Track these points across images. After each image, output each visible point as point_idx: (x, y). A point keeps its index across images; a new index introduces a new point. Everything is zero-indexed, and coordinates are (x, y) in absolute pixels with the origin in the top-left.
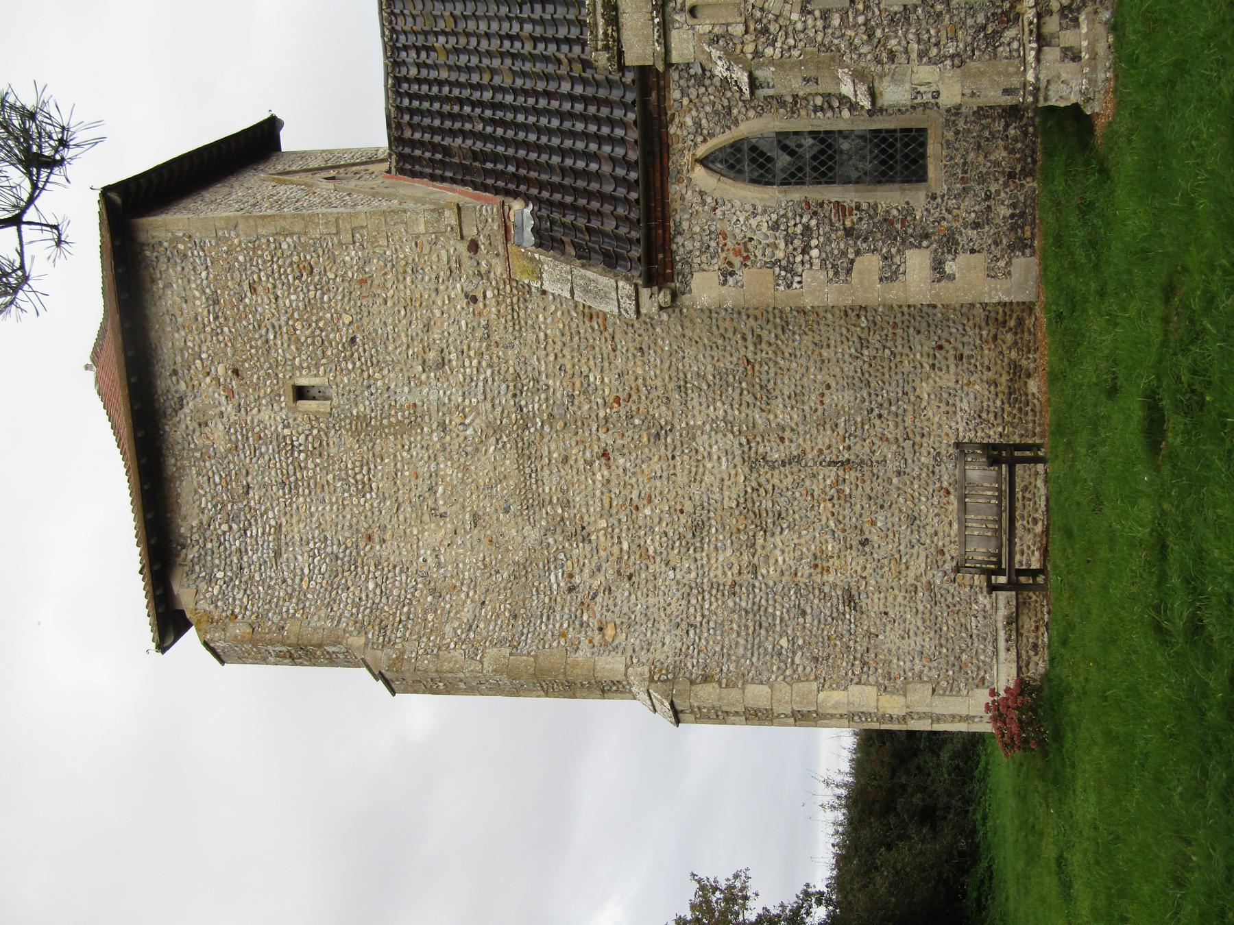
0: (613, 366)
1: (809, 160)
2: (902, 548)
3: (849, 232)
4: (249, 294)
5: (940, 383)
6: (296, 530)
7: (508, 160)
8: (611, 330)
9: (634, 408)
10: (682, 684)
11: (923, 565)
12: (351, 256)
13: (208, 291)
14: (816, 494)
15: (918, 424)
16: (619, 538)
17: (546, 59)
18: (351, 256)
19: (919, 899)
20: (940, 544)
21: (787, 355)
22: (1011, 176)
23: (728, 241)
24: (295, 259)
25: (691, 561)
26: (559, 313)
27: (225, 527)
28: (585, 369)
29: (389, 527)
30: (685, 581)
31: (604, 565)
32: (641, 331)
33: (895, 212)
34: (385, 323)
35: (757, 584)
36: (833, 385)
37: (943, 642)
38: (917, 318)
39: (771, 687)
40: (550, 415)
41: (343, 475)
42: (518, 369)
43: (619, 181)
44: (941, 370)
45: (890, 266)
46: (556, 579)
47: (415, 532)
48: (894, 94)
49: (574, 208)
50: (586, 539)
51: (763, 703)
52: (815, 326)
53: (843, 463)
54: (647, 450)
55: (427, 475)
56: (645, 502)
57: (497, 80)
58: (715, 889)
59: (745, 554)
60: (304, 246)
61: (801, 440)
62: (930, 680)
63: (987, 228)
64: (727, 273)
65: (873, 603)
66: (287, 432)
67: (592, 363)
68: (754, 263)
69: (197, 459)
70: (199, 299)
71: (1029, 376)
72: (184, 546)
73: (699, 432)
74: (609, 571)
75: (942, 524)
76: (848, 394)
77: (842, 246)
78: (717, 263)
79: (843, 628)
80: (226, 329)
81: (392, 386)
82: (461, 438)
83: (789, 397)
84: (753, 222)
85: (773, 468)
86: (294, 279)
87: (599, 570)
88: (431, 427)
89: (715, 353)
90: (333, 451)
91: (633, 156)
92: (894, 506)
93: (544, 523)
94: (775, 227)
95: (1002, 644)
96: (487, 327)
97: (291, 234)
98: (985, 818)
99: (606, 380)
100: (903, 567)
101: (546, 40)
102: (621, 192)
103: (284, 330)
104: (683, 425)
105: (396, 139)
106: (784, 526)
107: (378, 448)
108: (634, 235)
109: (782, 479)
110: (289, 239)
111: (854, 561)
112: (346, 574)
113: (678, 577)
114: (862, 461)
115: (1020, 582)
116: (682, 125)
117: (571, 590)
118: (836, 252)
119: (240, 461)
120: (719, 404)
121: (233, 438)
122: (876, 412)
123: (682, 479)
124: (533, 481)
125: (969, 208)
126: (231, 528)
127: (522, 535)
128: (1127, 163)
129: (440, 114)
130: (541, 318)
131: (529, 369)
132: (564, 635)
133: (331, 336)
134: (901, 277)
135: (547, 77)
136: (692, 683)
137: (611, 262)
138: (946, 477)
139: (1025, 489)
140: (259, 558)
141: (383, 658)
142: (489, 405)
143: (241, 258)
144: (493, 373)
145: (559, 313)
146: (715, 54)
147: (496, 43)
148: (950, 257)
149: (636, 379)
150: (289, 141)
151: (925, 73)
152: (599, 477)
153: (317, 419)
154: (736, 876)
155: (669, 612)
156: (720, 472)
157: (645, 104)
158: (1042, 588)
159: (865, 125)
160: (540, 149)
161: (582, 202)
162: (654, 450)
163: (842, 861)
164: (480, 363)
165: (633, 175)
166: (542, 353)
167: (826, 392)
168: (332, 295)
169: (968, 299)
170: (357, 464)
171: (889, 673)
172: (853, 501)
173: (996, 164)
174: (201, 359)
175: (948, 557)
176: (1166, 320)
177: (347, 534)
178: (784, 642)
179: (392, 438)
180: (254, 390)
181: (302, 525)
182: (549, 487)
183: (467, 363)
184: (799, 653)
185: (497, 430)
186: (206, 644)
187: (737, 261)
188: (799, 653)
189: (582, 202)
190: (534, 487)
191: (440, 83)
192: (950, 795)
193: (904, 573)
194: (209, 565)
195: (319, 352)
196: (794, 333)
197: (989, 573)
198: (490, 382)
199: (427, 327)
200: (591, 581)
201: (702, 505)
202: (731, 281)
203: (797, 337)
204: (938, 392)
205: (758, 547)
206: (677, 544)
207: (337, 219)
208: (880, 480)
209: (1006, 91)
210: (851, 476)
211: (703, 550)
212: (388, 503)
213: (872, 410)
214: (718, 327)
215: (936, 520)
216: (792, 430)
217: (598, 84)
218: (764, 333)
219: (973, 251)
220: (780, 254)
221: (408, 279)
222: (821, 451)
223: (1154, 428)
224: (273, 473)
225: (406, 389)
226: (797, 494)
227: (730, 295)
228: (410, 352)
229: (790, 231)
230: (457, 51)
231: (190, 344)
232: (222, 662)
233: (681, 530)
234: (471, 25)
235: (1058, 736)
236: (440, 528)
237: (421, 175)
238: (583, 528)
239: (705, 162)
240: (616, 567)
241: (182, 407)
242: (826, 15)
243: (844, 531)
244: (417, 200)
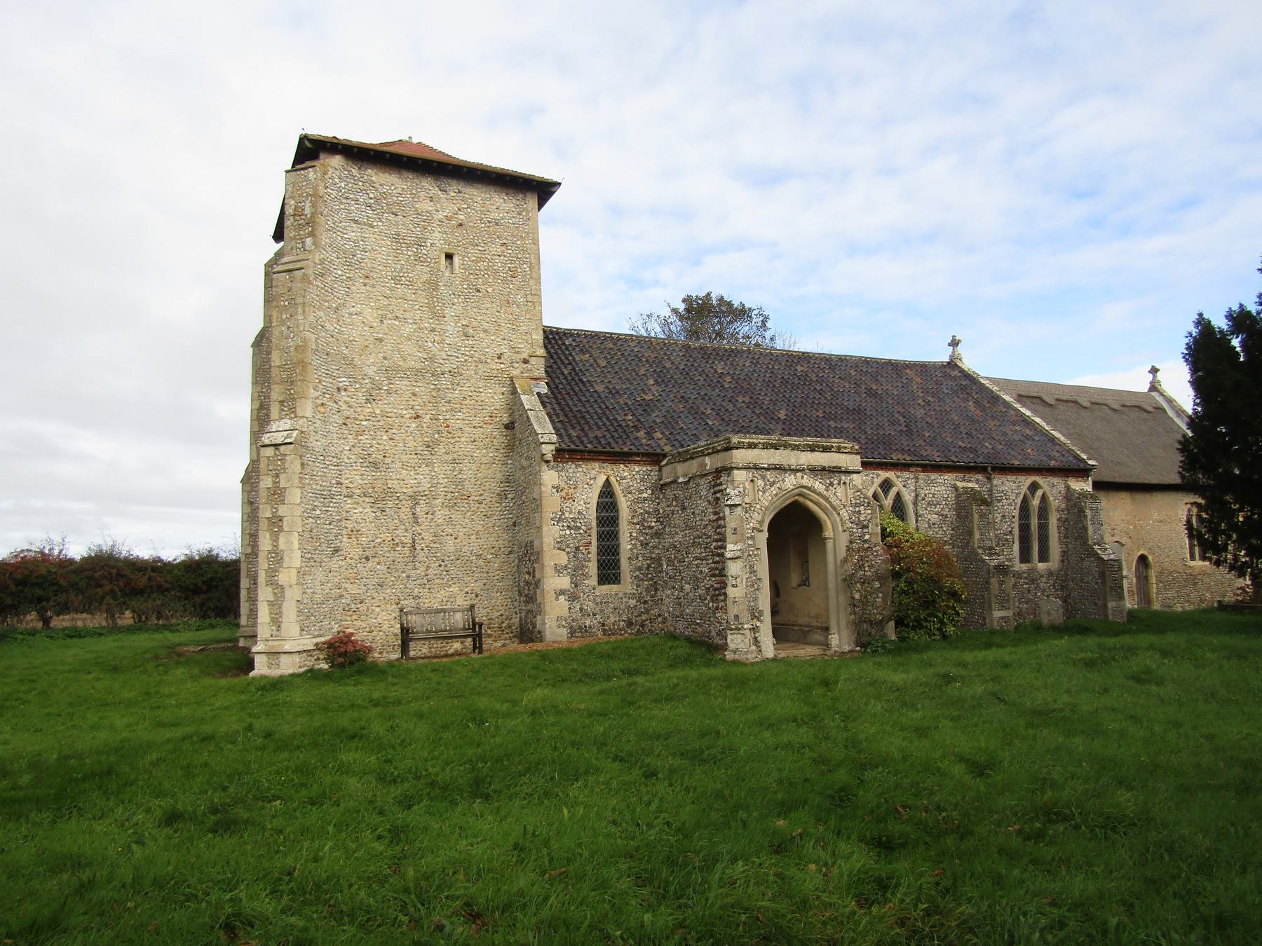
3: (577, 548)
50: (368, 401)
64: (558, 489)
65: (335, 564)
76: (452, 549)
78: (563, 485)
94: (580, 513)
109: (405, 513)
111: (356, 553)
123: (404, 458)
125: (589, 606)
127: (370, 365)
178: (318, 512)
187: (563, 494)
199: (485, 331)
210: (407, 551)
227: (547, 489)
239: (608, 482)
242: (752, 538)
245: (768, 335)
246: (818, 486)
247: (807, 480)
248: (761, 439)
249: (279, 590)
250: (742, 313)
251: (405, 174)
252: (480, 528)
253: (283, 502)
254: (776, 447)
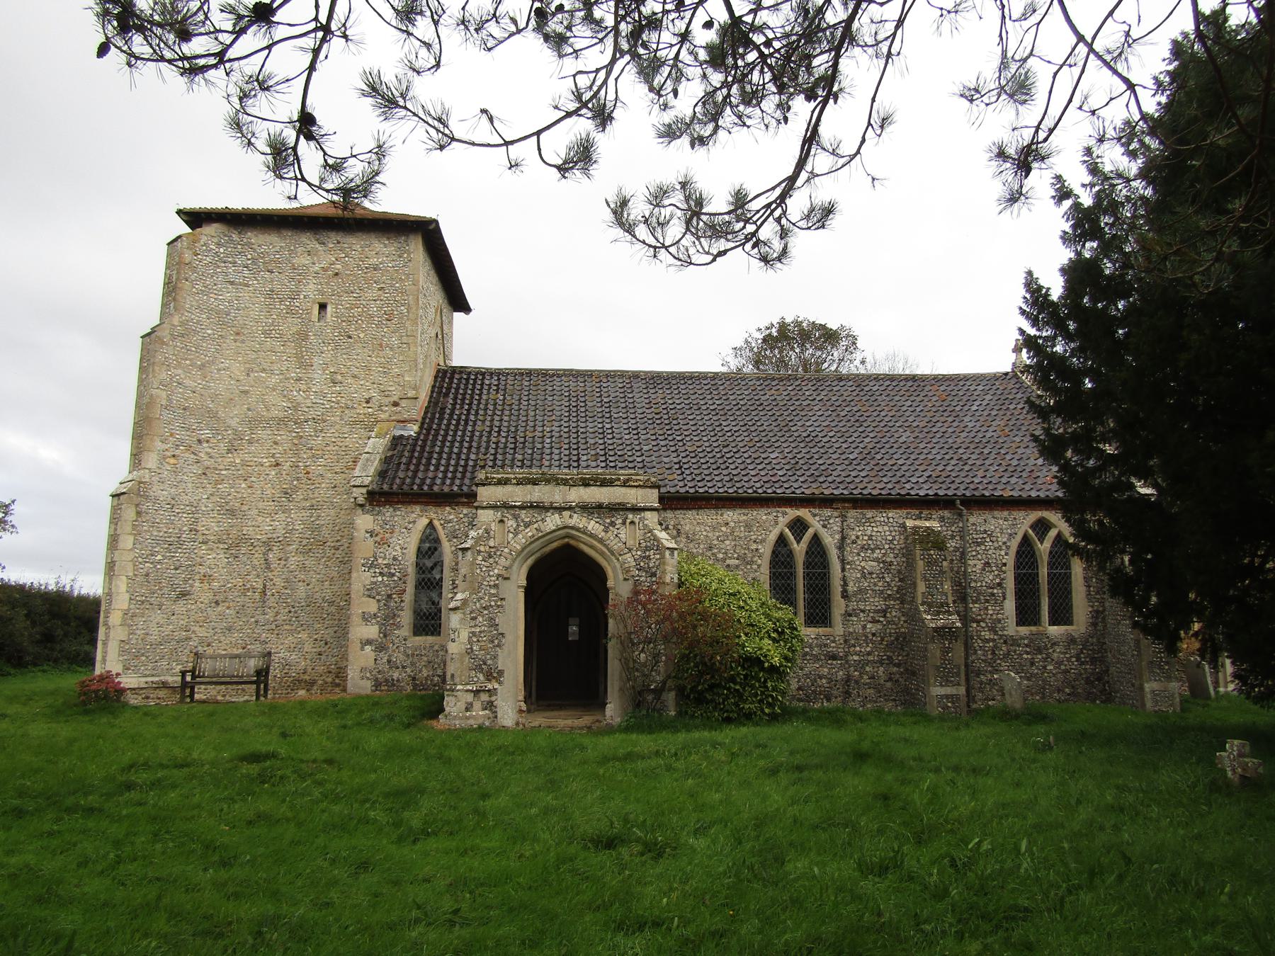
1: (429, 576)
3: (389, 596)
7: (439, 425)
10: (136, 500)
12: (395, 341)
17: (487, 448)
18: (395, 341)
19: (25, 633)
22: (414, 679)
38: (342, 632)
43: (423, 480)
46: (206, 433)
48: (454, 620)
49: (411, 457)
50: (229, 451)
51: (121, 545)
57: (479, 423)
58: (6, 514)
62: (130, 639)
65: (180, 607)
75: (226, 644)
78: (377, 529)
79: (166, 590)
84: (398, 548)
90: (290, 320)
91: (436, 488)
94: (395, 559)
95: (150, 679)
98: (44, 671)
101: (496, 449)
102: (418, 481)
105: (454, 370)
108: (395, 487)
109: (257, 559)
111: (207, 597)
115: (186, 688)
116: (450, 513)
117: (199, 441)
123: (261, 505)
125: (398, 657)
127: (234, 418)
128: (407, 738)
129: (465, 393)
132: (172, 435)
135: (478, 448)
136: (137, 505)
137: (382, 474)
139: (243, 690)
141: (165, 333)
146: (480, 531)
147: (497, 424)
150: (458, 316)
151: (464, 635)
154: (13, 526)
156: (262, 525)
157: (461, 495)
158: (182, 701)
159: (443, 603)
160: (443, 442)
161: (414, 461)
163: (21, 588)
165: (426, 488)
169: (350, 658)
173: (420, 671)
176: (314, 761)
178: (159, 557)
182: (262, 434)
185: (295, 409)
186: (179, 237)
187: (378, 539)
189: (414, 461)
191: (480, 395)
192: (61, 651)
197: (193, 671)
199: (354, 377)
204: (302, 643)
209: (453, 676)
217: (473, 473)
220: (380, 561)
223: (255, 758)
227: (360, 534)
230: (495, 405)
232: (169, 244)
234: (507, 413)
235: (86, 712)
237: (435, 381)
239: (431, 524)
242: (496, 586)
244: (422, 377)
245: (858, 356)
246: (593, 526)
247: (577, 520)
248: (520, 472)
250: (830, 337)
251: (285, 233)
252: (335, 574)
254: (534, 482)
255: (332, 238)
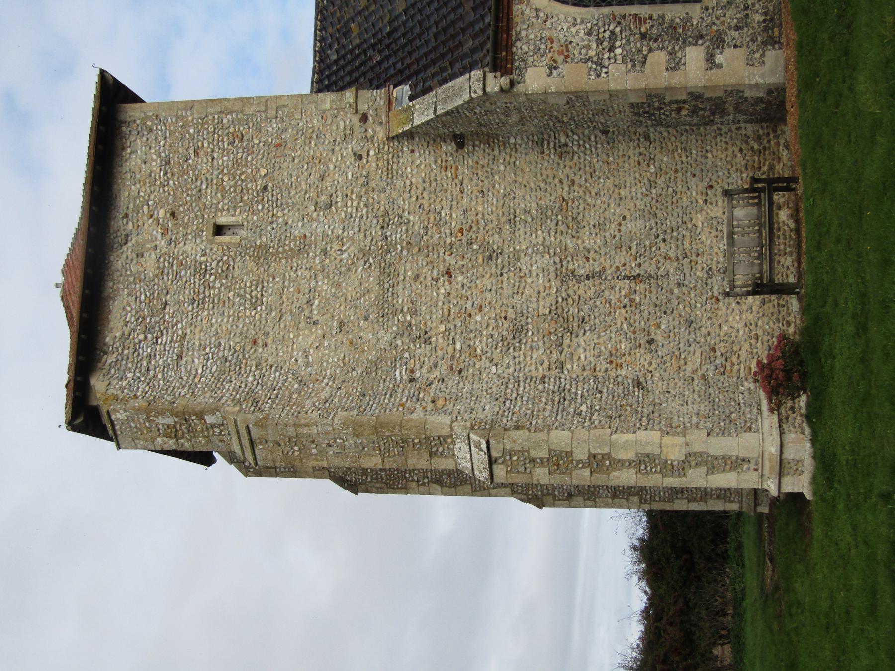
0: (460, 205)
2: (681, 346)
3: (643, 36)
4: (193, 156)
5: (712, 214)
6: (197, 337)
8: (460, 178)
9: (474, 237)
11: (699, 360)
12: (273, 127)
13: (163, 154)
14: (613, 302)
15: (694, 246)
16: (454, 339)
18: (273, 127)
20: (712, 342)
21: (593, 194)
23: (554, 45)
24: (232, 130)
25: (510, 358)
26: (422, 166)
27: (141, 337)
28: (438, 207)
29: (272, 333)
30: (505, 375)
31: (440, 363)
32: (483, 179)
33: (678, 20)
34: (291, 175)
35: (563, 376)
36: (628, 217)
37: (715, 407)
39: (572, 433)
40: (409, 243)
41: (242, 292)
42: (387, 207)
44: (711, 204)
45: (674, 59)
46: (401, 373)
47: (292, 336)
50: (427, 341)
52: (615, 173)
53: (635, 278)
54: (481, 269)
55: (307, 291)
56: (477, 311)
59: (554, 352)
60: (239, 121)
61: (602, 260)
63: (746, 30)
64: (552, 67)
65: (657, 386)
66: (204, 259)
67: (444, 202)
68: (573, 59)
69: (130, 283)
70: (155, 160)
71: (779, 208)
72: (106, 353)
73: (523, 255)
74: (444, 368)
76: (640, 223)
77: (639, 45)
78: (546, 60)
80: (171, 182)
81: (290, 222)
82: (337, 262)
83: (594, 226)
84: (574, 30)
85: (580, 282)
86: (228, 144)
87: (435, 366)
88: (315, 253)
89: (539, 194)
92: (675, 312)
93: (395, 328)
96: (367, 177)
97: (231, 113)
99: (454, 215)
100: (682, 362)
103: (215, 182)
104: (511, 249)
106: (587, 328)
107: (272, 270)
109: (586, 290)
110: (229, 117)
111: (642, 358)
112: (232, 373)
113: (500, 371)
114: (650, 276)
117: (412, 380)
118: (634, 50)
119: (164, 283)
120: (539, 232)
121: (161, 265)
122: (662, 236)
123: (507, 291)
124: (390, 294)
126: (146, 338)
127: (377, 337)
130: (409, 170)
131: (396, 207)
133: (249, 186)
134: (682, 67)
136: (506, 430)
138: (716, 288)
140: (164, 362)
142: (362, 235)
143: (192, 131)
144: (368, 211)
145: (422, 166)
148: (719, 51)
149: (477, 214)
152: (442, 291)
153: (229, 248)
155: (490, 391)
162: (487, 269)
164: (359, 204)
166: (406, 196)
167: (623, 222)
168: (254, 156)
170: (254, 283)
171: (671, 424)
172: (642, 308)
174: (148, 205)
175: (718, 354)
177: (238, 340)
178: (584, 408)
179: (284, 261)
180: (184, 228)
181: (202, 334)
183: (349, 204)
184: (596, 413)
187: (560, 59)
188: (596, 413)
190: (390, 299)
193: (683, 368)
194: (123, 368)
195: (238, 198)
196: (599, 178)
198: (365, 218)
199: (322, 178)
200: (428, 375)
201: (522, 312)
202: (555, 72)
203: (602, 181)
205: (565, 346)
206: (500, 344)
207: (267, 101)
208: (664, 290)
210: (641, 287)
211: (520, 350)
212: (274, 314)
213: (658, 236)
214: (542, 175)
215: (708, 322)
216: (596, 251)
218: (577, 179)
219: (736, 46)
220: (592, 53)
221: (313, 143)
222: (617, 268)
224: (187, 292)
225: (300, 224)
226: (598, 303)
227: (553, 84)
228: (307, 196)
229: (600, 36)
231: (142, 194)
233: (504, 333)
236: (312, 333)
238: (426, 333)
240: (449, 363)
241: (126, 243)
243: (635, 332)
249: (691, 459)
252: (609, 183)
253: (569, 454)
255: (121, 225)
